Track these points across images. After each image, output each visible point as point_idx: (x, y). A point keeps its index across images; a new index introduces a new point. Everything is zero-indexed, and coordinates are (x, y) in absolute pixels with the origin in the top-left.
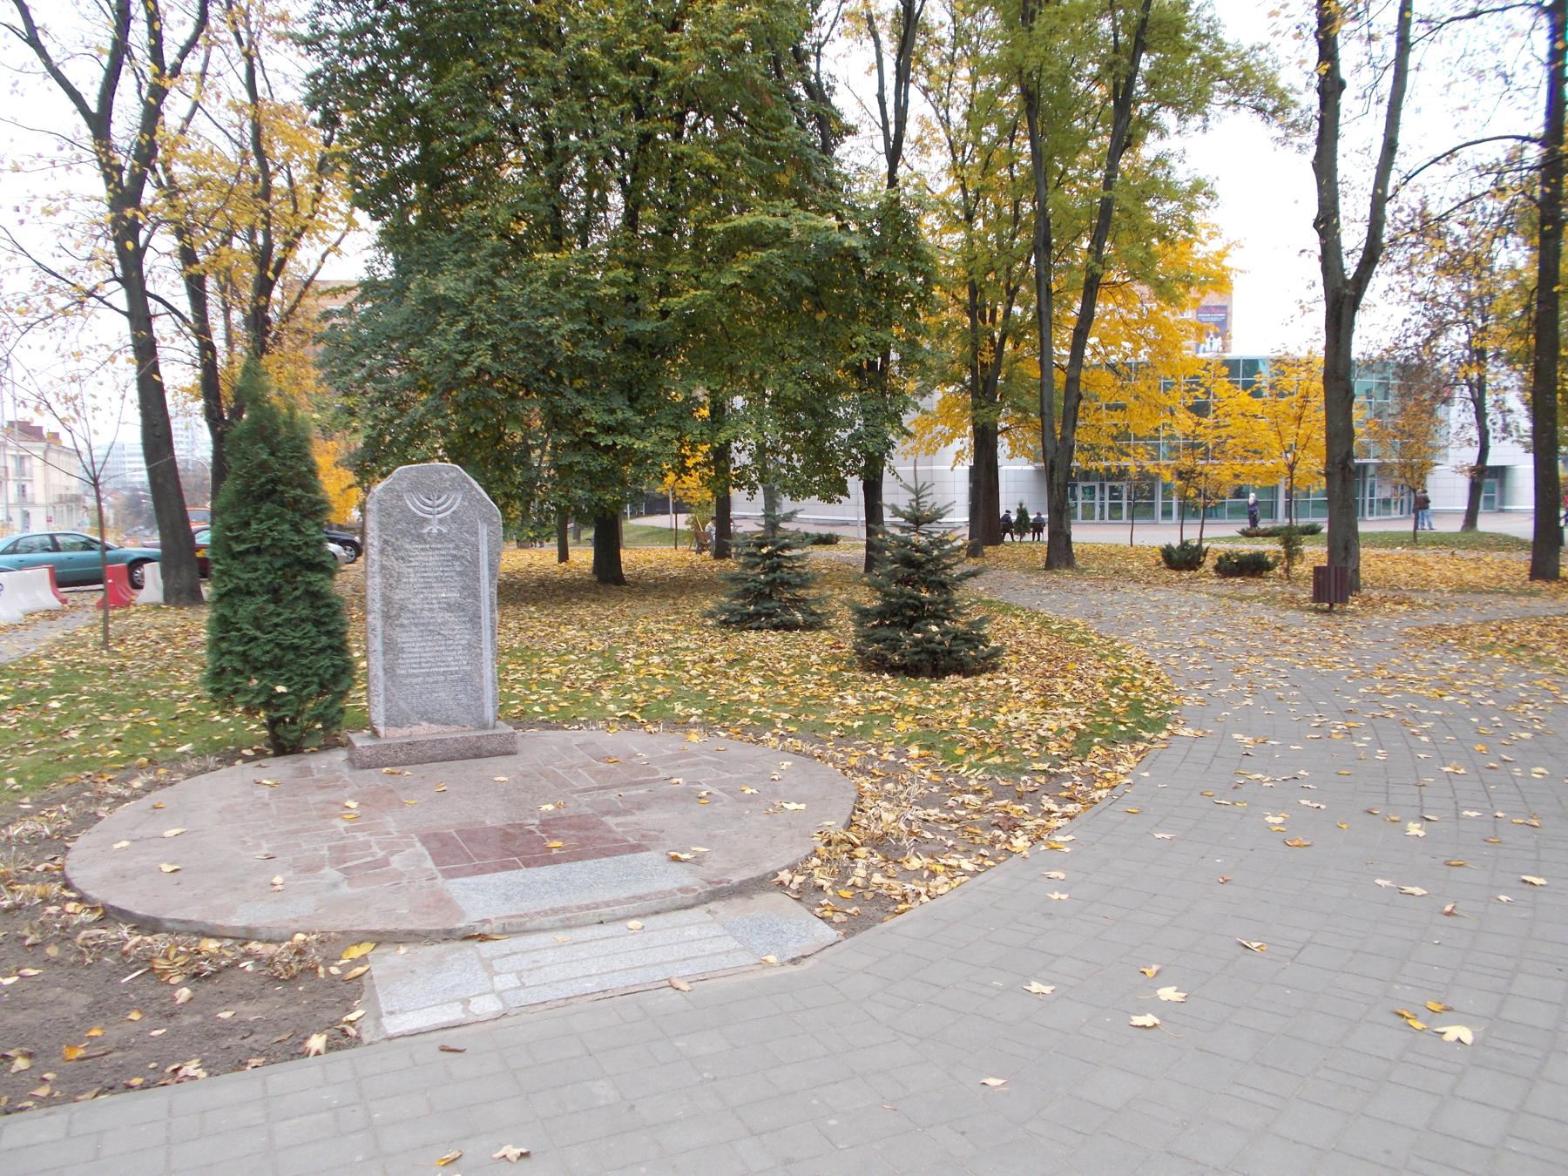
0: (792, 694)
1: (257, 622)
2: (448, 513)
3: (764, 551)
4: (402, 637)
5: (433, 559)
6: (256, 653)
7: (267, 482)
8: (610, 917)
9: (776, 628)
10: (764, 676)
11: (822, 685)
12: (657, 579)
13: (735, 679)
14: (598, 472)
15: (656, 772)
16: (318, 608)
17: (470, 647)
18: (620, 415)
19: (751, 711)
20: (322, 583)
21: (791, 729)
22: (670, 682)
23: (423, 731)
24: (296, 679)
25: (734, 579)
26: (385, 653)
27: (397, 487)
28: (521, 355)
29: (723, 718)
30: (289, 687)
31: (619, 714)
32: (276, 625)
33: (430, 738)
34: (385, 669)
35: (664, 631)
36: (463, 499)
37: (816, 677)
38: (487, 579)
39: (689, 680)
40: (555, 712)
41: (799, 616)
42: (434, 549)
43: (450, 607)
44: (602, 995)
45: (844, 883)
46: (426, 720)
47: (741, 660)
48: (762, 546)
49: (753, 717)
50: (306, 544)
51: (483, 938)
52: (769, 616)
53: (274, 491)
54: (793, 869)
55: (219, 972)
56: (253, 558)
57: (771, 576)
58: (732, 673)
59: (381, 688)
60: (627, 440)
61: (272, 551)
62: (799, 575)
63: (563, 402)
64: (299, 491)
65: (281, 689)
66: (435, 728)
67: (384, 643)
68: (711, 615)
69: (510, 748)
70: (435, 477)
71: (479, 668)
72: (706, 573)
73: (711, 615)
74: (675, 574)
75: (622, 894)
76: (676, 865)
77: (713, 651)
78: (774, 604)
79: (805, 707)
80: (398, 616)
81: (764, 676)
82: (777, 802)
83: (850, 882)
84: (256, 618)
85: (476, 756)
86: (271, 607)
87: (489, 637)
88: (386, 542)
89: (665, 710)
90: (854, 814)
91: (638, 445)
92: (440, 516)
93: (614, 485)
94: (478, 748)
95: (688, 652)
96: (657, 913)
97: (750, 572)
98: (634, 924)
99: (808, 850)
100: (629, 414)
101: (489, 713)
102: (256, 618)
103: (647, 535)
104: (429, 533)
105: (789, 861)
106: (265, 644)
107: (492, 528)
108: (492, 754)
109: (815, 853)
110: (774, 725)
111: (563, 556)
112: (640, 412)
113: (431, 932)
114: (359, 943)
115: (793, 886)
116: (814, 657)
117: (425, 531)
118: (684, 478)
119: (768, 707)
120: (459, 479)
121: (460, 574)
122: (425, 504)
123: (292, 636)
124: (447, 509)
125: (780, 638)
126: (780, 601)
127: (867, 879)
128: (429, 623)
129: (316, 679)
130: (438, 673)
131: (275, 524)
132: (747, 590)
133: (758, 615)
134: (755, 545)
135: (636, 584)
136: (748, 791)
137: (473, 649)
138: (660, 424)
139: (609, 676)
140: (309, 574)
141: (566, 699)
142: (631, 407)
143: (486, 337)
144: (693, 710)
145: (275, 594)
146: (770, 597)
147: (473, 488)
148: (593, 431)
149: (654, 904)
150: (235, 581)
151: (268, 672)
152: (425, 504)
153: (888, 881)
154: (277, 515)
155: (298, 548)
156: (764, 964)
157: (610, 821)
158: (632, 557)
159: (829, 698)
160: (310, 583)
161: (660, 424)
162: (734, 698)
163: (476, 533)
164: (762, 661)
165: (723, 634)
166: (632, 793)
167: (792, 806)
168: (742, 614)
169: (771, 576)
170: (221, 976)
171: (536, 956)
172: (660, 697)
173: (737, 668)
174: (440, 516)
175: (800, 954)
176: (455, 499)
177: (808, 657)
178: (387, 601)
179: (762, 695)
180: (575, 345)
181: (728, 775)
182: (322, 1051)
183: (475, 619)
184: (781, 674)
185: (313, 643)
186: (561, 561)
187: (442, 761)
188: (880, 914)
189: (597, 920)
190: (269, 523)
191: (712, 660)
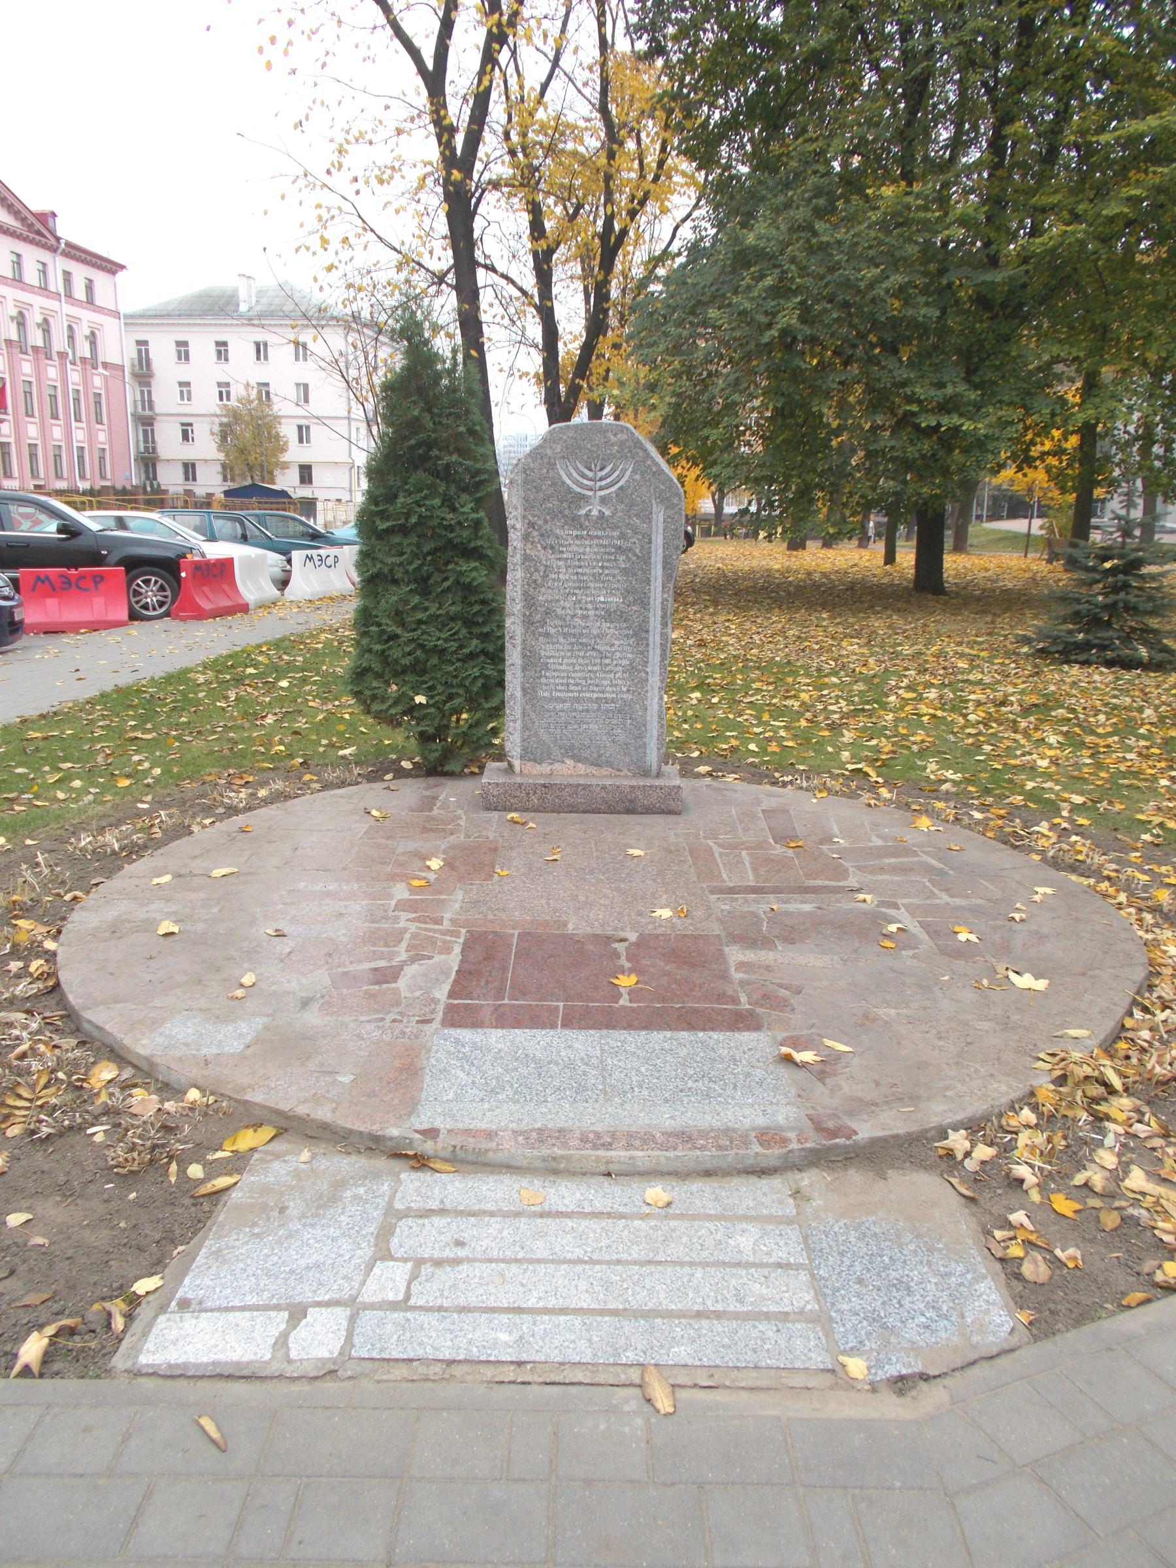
0: (1099, 766)
1: (399, 616)
2: (613, 489)
3: (1107, 565)
4: (547, 650)
5: (590, 551)
6: (396, 653)
7: (419, 445)
8: (624, 1168)
9: (1109, 664)
10: (1065, 734)
11: (1147, 757)
12: (984, 590)
13: (1026, 733)
14: (915, 460)
15: (844, 874)
16: (471, 604)
17: (632, 668)
18: (949, 390)
19: (1030, 785)
20: (474, 574)
21: (1081, 821)
22: (937, 727)
23: (567, 771)
24: (440, 689)
25: (1064, 599)
26: (524, 668)
27: (549, 452)
28: (835, 315)
29: (987, 791)
30: (432, 697)
31: (850, 767)
32: (420, 622)
33: (572, 781)
34: (524, 690)
35: (962, 655)
36: (634, 472)
37: (1142, 743)
38: (660, 581)
39: (963, 727)
40: (774, 753)
41: (1143, 652)
42: (592, 538)
43: (609, 615)
44: (510, 1374)
45: (1070, 1177)
46: (573, 757)
47: (1041, 709)
48: (1106, 559)
49: (1031, 796)
50: (460, 523)
51: (420, 1162)
52: (1102, 648)
53: (425, 458)
54: (974, 1127)
55: (61, 1135)
56: (396, 539)
57: (1112, 598)
58: (1023, 724)
59: (518, 713)
60: (955, 420)
61: (419, 530)
62: (1151, 599)
63: (883, 374)
64: (455, 457)
65: (420, 699)
66: (582, 768)
67: (524, 656)
68: (1026, 640)
69: (672, 805)
70: (599, 439)
71: (642, 698)
72: (1047, 585)
73: (1026, 640)
74: (1010, 585)
75: (666, 1119)
76: (783, 1071)
77: (1010, 690)
78: (1111, 633)
79: (1111, 790)
80: (543, 623)
81: (1065, 734)
82: (1001, 968)
83: (1079, 1179)
84: (398, 613)
85: (628, 812)
86: (416, 599)
87: (658, 658)
88: (531, 525)
89: (914, 767)
90: (1131, 1015)
91: (967, 426)
92: (602, 493)
93: (933, 476)
94: (631, 801)
95: (977, 689)
96: (708, 1174)
97: (1084, 590)
98: (657, 1192)
99: (1017, 1090)
100: (961, 388)
101: (652, 757)
102: (398, 613)
103: (999, 540)
104: (587, 515)
105: (974, 1108)
106: (406, 644)
107: (671, 512)
108: (648, 811)
109: (1030, 1099)
110: (1057, 811)
111: (890, 558)
112: (976, 387)
113: (351, 1132)
114: (257, 1126)
115: (971, 1165)
116: (1148, 712)
117: (583, 512)
118: (1026, 470)
119: (1057, 782)
120: (630, 443)
121: (624, 572)
122: (583, 476)
123: (435, 637)
124: (582, 486)
125: (1111, 678)
126: (1122, 629)
127: (1118, 1175)
128: (581, 634)
129: (461, 691)
130: (590, 700)
131: (425, 498)
132: (1077, 613)
133: (1086, 646)
134: (1097, 557)
135: (957, 595)
136: (963, 937)
137: (637, 671)
138: (1001, 402)
139: (863, 710)
140: (461, 562)
141: (795, 737)
142: (967, 380)
143: (795, 293)
144: (949, 774)
145: (423, 585)
146: (1108, 624)
147: (648, 455)
148: (914, 408)
149: (707, 1156)
150: (379, 566)
151: (409, 677)
152: (583, 476)
153: (1160, 1190)
154: (429, 487)
155: (451, 529)
156: (836, 1372)
157: (735, 954)
158: (953, 564)
159: (1154, 779)
160: (461, 573)
161: (1001, 402)
162: (1013, 762)
163: (648, 518)
164: (1073, 711)
165: (1036, 666)
166: (792, 907)
167: (1025, 981)
168: (1067, 644)
169: (1112, 598)
170: (59, 1142)
171: (467, 1228)
172: (915, 748)
173: (1032, 719)
174: (602, 493)
175: (918, 1367)
176: (624, 471)
177: (1141, 710)
178: (529, 601)
179: (1054, 761)
180: (906, 303)
181: (945, 898)
182: (35, 1368)
183: (641, 633)
184: (1093, 733)
185: (461, 647)
186: (886, 563)
187: (584, 812)
188: (1121, 1278)
189: (603, 1168)
190: (418, 496)
191: (1003, 703)
